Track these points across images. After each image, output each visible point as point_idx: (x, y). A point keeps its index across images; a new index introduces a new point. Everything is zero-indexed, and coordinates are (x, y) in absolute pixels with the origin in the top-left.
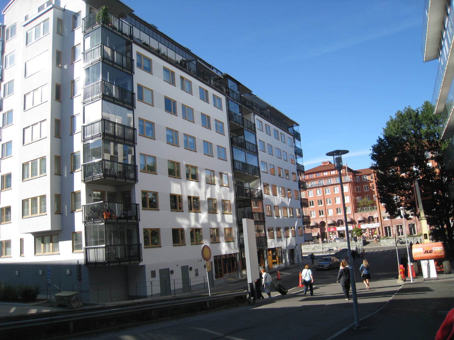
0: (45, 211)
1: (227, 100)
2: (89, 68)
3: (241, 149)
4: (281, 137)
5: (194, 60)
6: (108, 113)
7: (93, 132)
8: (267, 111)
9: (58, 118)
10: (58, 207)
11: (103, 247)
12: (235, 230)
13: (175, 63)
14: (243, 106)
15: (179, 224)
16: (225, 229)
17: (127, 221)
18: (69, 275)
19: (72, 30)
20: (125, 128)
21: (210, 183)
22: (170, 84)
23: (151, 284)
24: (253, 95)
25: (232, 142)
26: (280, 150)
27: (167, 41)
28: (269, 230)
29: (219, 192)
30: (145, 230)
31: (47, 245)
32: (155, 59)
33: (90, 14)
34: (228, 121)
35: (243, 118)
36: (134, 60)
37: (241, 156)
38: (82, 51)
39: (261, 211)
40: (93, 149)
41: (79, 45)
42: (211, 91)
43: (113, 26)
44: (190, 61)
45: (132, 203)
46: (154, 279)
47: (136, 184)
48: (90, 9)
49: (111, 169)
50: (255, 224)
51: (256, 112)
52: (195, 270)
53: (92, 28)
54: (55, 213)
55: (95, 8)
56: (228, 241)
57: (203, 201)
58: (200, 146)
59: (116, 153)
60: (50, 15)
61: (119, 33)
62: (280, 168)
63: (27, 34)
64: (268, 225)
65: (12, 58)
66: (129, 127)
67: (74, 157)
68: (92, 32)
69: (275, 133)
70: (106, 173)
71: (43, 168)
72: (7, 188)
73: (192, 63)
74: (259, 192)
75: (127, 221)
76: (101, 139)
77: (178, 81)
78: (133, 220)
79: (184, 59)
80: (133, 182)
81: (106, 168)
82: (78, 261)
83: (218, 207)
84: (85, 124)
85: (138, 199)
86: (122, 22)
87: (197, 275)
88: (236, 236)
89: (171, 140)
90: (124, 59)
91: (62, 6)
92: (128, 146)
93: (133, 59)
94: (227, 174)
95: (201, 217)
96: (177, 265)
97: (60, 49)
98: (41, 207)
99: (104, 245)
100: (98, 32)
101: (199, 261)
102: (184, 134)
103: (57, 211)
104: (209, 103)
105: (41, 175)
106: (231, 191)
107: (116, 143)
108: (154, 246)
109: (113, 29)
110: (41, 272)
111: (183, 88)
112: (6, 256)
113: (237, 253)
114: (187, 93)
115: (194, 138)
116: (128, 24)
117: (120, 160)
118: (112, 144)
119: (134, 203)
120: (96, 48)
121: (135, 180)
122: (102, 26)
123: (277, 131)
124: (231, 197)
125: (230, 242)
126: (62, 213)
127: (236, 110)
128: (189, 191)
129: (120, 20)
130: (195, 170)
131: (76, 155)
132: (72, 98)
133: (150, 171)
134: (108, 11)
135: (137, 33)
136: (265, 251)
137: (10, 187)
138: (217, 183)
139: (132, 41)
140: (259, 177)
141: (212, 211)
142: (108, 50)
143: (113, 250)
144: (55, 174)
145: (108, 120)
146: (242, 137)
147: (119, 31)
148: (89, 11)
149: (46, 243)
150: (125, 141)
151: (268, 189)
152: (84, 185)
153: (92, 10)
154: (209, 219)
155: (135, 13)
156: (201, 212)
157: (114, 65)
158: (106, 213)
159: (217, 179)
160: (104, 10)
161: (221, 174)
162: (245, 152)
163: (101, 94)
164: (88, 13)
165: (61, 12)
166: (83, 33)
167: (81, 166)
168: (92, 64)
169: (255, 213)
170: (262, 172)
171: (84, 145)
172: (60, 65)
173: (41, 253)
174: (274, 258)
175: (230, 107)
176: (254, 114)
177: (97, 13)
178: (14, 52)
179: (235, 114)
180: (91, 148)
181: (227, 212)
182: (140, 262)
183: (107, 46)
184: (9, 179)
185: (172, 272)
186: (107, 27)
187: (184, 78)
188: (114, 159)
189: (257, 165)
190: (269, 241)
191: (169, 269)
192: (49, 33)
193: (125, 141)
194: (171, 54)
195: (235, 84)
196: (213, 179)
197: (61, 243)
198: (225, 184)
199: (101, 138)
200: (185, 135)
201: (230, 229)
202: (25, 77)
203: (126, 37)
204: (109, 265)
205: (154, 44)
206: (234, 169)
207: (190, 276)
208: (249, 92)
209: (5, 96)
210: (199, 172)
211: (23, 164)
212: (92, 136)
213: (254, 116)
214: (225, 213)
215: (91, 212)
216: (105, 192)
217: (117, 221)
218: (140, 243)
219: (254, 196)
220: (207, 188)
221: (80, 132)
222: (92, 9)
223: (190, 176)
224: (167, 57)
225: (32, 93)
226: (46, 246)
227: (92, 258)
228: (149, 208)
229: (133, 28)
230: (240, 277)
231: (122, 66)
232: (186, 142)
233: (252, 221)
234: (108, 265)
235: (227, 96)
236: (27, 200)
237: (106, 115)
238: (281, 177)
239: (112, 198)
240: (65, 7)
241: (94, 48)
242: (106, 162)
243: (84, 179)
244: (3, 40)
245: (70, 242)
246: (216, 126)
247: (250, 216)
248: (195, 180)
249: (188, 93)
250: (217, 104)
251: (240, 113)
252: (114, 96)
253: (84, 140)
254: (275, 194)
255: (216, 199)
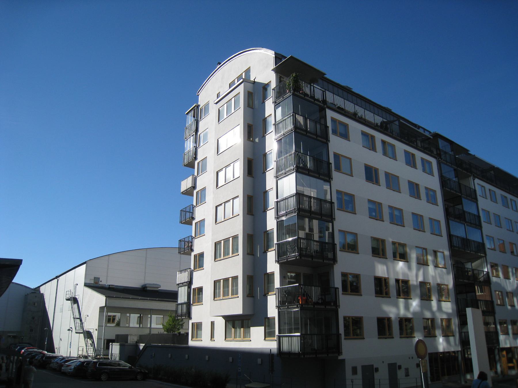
0: (237, 293)
1: (439, 164)
2: (281, 139)
3: (459, 221)
4: (512, 205)
5: (396, 121)
6: (303, 186)
7: (287, 207)
8: (491, 173)
9: (251, 194)
10: (250, 290)
11: (297, 336)
12: (455, 322)
13: (375, 126)
14: (459, 169)
15: (385, 312)
16: (442, 320)
17: (325, 307)
18: (207, 360)
19: (262, 102)
20: (322, 202)
21: (422, 263)
22: (369, 149)
23: (352, 382)
24: (470, 154)
25: (448, 214)
26: (511, 220)
27: (363, 103)
28: (501, 324)
29: (433, 274)
30: (345, 318)
31: (238, 330)
32: (353, 125)
33: (280, 83)
34: (441, 189)
35: (460, 184)
36: (328, 127)
37: (459, 231)
38: (273, 122)
39: (488, 298)
40: (288, 225)
41: (270, 116)
42: (419, 155)
43: (305, 93)
44: (392, 122)
45: (330, 286)
46: (354, 377)
47: (335, 264)
48: (280, 77)
49: (307, 248)
50: (483, 315)
51: (475, 175)
52: (405, 369)
53: (283, 97)
54: (247, 296)
55: (285, 77)
56: (446, 336)
57: (414, 286)
58: (408, 219)
59: (311, 230)
60: (241, 89)
61: (311, 100)
62: (511, 244)
63: (219, 110)
64: (499, 316)
65: (206, 136)
66: (326, 201)
67: (267, 235)
68: (282, 102)
69: (502, 200)
70: (302, 252)
71: (235, 247)
72: (199, 268)
73: (394, 124)
74: (485, 274)
75: (325, 307)
76: (295, 215)
77: (379, 146)
78: (331, 306)
79: (385, 120)
80: (332, 262)
81: (302, 247)
82: (271, 350)
83: (432, 293)
84: (278, 200)
85: (338, 283)
86: (314, 87)
87: (407, 375)
88: (457, 330)
89: (374, 214)
90: (318, 126)
91: (252, 79)
92: (326, 222)
93: (328, 125)
94: (443, 253)
95: (412, 305)
96: (383, 362)
97: (251, 123)
98: (232, 288)
99: (299, 334)
100: (289, 101)
101: (409, 358)
102: (413, 214)
103: (249, 294)
104: (417, 169)
105: (233, 255)
106: (448, 273)
107: (311, 219)
108: (355, 337)
109: (315, 101)
110: (231, 359)
111: (385, 153)
112: (197, 339)
113: (458, 351)
114: (390, 159)
115: (401, 211)
116: (320, 88)
117: (316, 237)
118: (307, 220)
119: (332, 286)
120: (288, 118)
121: (334, 260)
122: (293, 94)
123: (506, 197)
124: (449, 281)
125: (448, 336)
126: (254, 296)
127: (451, 175)
128: (397, 273)
129: (312, 86)
130: (404, 248)
131: (269, 232)
132: (264, 173)
133: (350, 249)
134: (298, 78)
135: (330, 97)
136: (496, 352)
137: (203, 267)
138: (430, 263)
139: (325, 106)
140: (484, 255)
141: (425, 297)
142: (300, 119)
143: (310, 340)
144: (248, 254)
145: (302, 194)
146: (459, 207)
147: (311, 97)
148: (279, 81)
149: (236, 328)
150: (322, 217)
151: (497, 271)
152: (278, 266)
153: (282, 79)
154: (422, 306)
155: (327, 76)
156: (411, 299)
157: (308, 134)
158: (302, 297)
159: (430, 258)
160: (295, 77)
161: (435, 252)
162: (465, 225)
163: (295, 166)
164: (278, 82)
165: (251, 85)
166: (274, 104)
167: (275, 245)
168: (284, 135)
169: (480, 300)
170: (488, 248)
171: (278, 222)
172: (251, 139)
173: (232, 339)
174: (510, 360)
175: (443, 172)
176: (473, 178)
177: (288, 81)
178: (208, 130)
179: (449, 179)
180: (285, 224)
181: (444, 298)
182: (339, 355)
183: (299, 115)
184: (201, 258)
185: (377, 370)
186: (298, 94)
187: (385, 142)
188: (309, 237)
189: (480, 240)
190: (502, 337)
191: (373, 366)
192: (240, 108)
193: (322, 217)
194: (369, 116)
195: (448, 144)
196: (425, 258)
197: (253, 329)
198: (440, 264)
199: (296, 214)
200: (390, 207)
201: (449, 320)
202: (217, 154)
203: (319, 103)
204: (304, 356)
205: (350, 107)
206: (451, 246)
207: (399, 377)
208: (466, 151)
209: (199, 174)
210: (408, 250)
211: (215, 243)
212: (286, 212)
213: (474, 180)
214: (442, 300)
215: (285, 296)
216: (300, 273)
217: (314, 306)
218: (340, 333)
219: (479, 279)
220: (418, 270)
221: (274, 208)
222: (281, 78)
223: (398, 255)
224: (365, 120)
225: (224, 169)
226: (236, 330)
227: (285, 347)
228: (349, 293)
229: (325, 92)
230: (463, 383)
231: (316, 135)
232: (391, 215)
233: (479, 312)
234: (303, 357)
235: (438, 159)
236: (219, 281)
237: (301, 188)
238: (515, 255)
239: (308, 280)
240: (254, 79)
241: (286, 118)
242: (301, 240)
243: (278, 259)
244: (197, 119)
245: (262, 328)
246: (427, 195)
247: (475, 304)
248: (405, 260)
249: (391, 159)
250: (427, 168)
251: (455, 177)
252: (309, 168)
253: (278, 217)
254: (507, 277)
255: (430, 283)
